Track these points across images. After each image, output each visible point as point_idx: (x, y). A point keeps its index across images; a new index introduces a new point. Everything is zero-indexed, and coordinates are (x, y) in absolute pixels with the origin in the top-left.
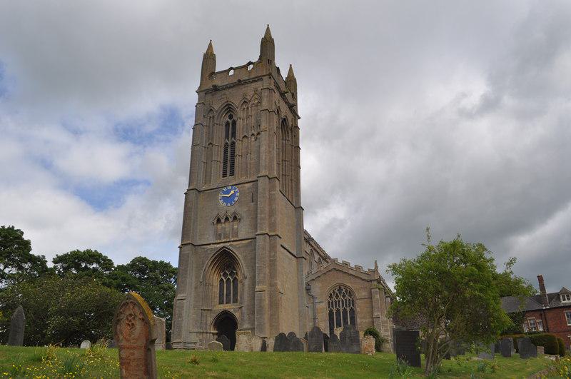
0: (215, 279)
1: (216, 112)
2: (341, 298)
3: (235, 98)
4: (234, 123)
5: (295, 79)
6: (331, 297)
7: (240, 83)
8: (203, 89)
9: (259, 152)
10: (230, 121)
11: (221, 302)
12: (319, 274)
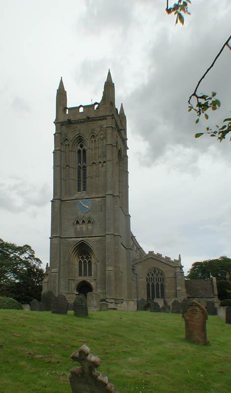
0: (76, 261)
1: (71, 141)
2: (155, 276)
3: (83, 130)
4: (84, 151)
5: (125, 117)
6: (148, 275)
7: (88, 119)
8: (60, 121)
9: (105, 176)
10: (82, 150)
11: (80, 275)
12: (141, 261)
